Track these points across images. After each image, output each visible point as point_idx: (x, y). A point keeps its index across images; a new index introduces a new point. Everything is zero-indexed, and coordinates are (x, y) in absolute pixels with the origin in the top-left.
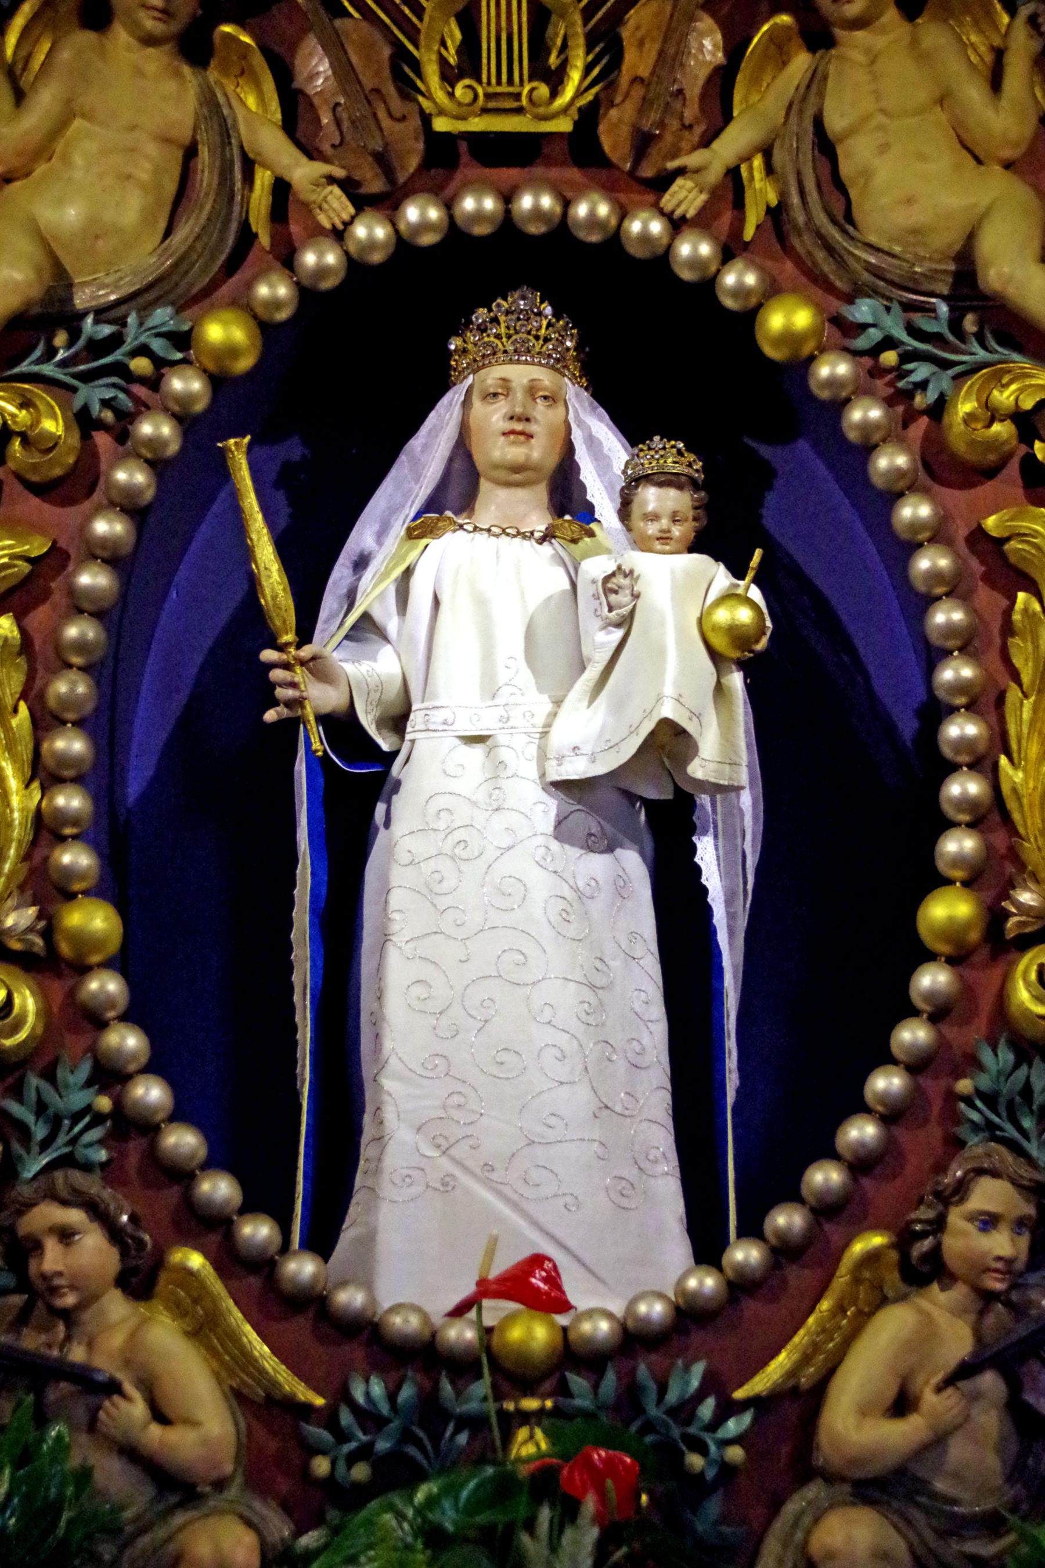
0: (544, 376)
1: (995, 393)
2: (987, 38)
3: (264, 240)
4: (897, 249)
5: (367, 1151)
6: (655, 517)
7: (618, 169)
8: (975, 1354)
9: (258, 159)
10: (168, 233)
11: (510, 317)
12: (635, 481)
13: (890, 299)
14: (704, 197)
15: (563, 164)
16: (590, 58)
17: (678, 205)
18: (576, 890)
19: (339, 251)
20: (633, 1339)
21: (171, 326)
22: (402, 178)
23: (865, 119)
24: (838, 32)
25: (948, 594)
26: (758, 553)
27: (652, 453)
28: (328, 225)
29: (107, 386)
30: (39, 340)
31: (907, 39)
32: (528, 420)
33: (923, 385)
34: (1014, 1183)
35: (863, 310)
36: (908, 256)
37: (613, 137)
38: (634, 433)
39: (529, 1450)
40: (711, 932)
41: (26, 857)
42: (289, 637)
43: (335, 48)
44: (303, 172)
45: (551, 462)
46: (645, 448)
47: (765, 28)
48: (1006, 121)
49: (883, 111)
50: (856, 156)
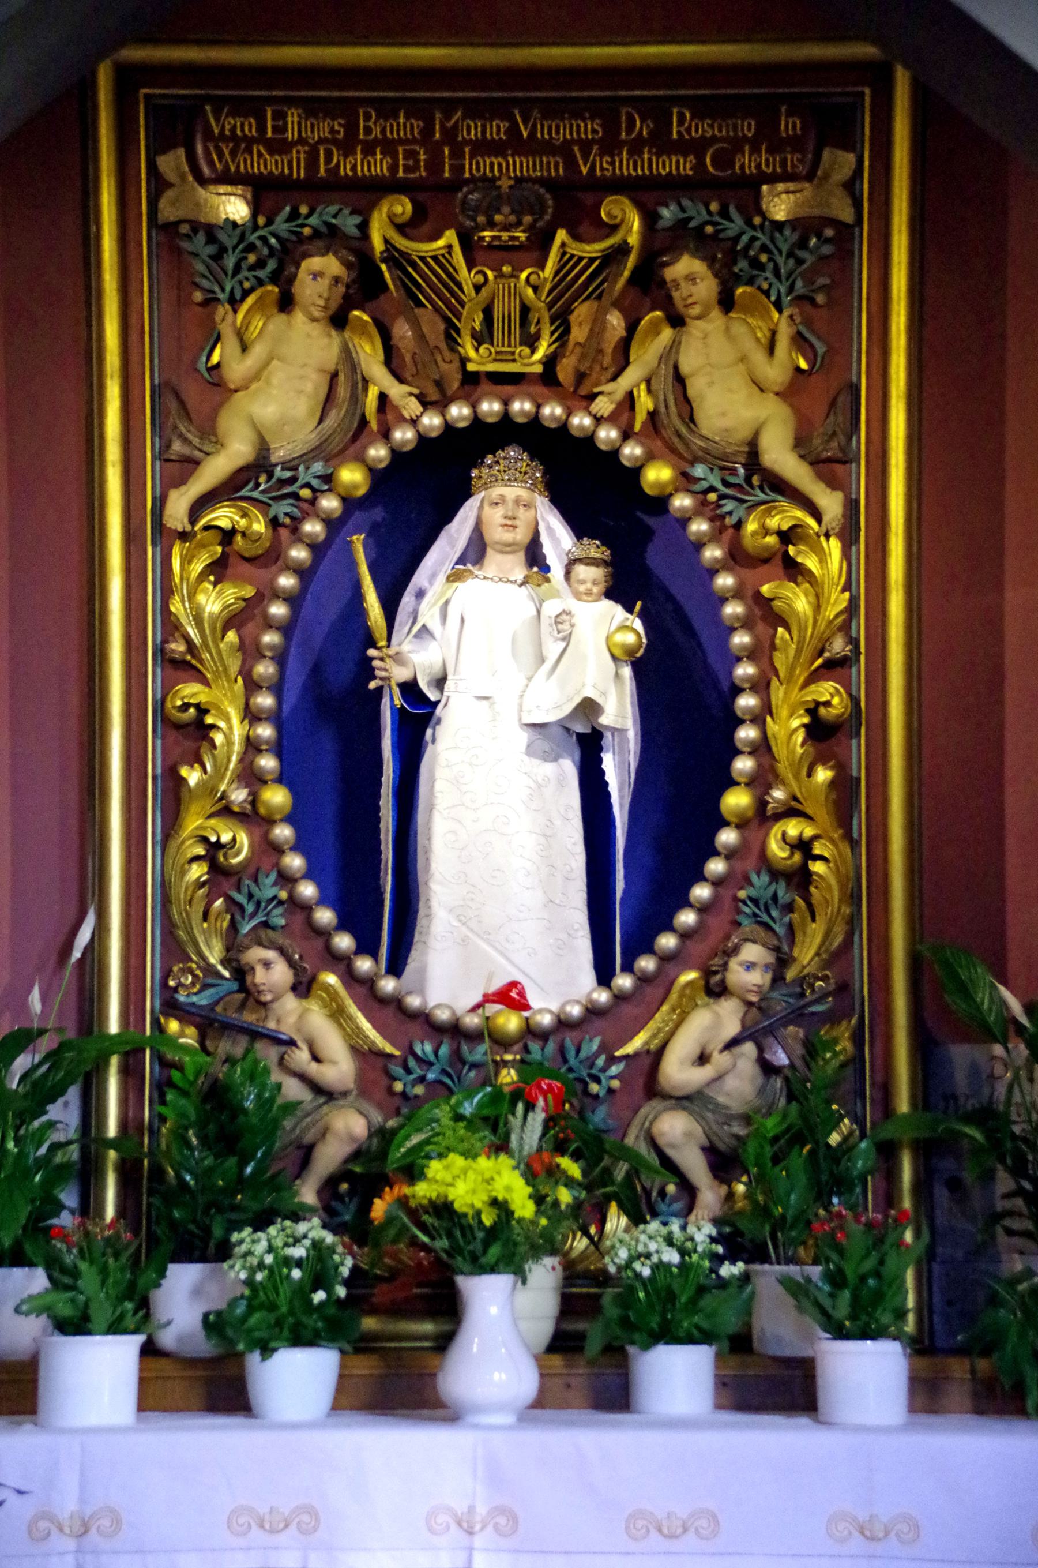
1: (768, 521)
3: (374, 425)
4: (717, 439)
5: (421, 921)
6: (583, 582)
8: (741, 1032)
10: (321, 421)
16: (553, 328)
18: (536, 782)
20: (563, 1023)
22: (449, 393)
24: (688, 320)
25: (742, 627)
31: (723, 327)
33: (730, 513)
34: (763, 945)
35: (699, 471)
36: (723, 443)
37: (565, 371)
39: (508, 1080)
40: (609, 806)
41: (241, 761)
42: (383, 643)
43: (415, 324)
44: (396, 391)
45: (527, 540)
48: (775, 372)
49: (710, 364)
50: (695, 387)
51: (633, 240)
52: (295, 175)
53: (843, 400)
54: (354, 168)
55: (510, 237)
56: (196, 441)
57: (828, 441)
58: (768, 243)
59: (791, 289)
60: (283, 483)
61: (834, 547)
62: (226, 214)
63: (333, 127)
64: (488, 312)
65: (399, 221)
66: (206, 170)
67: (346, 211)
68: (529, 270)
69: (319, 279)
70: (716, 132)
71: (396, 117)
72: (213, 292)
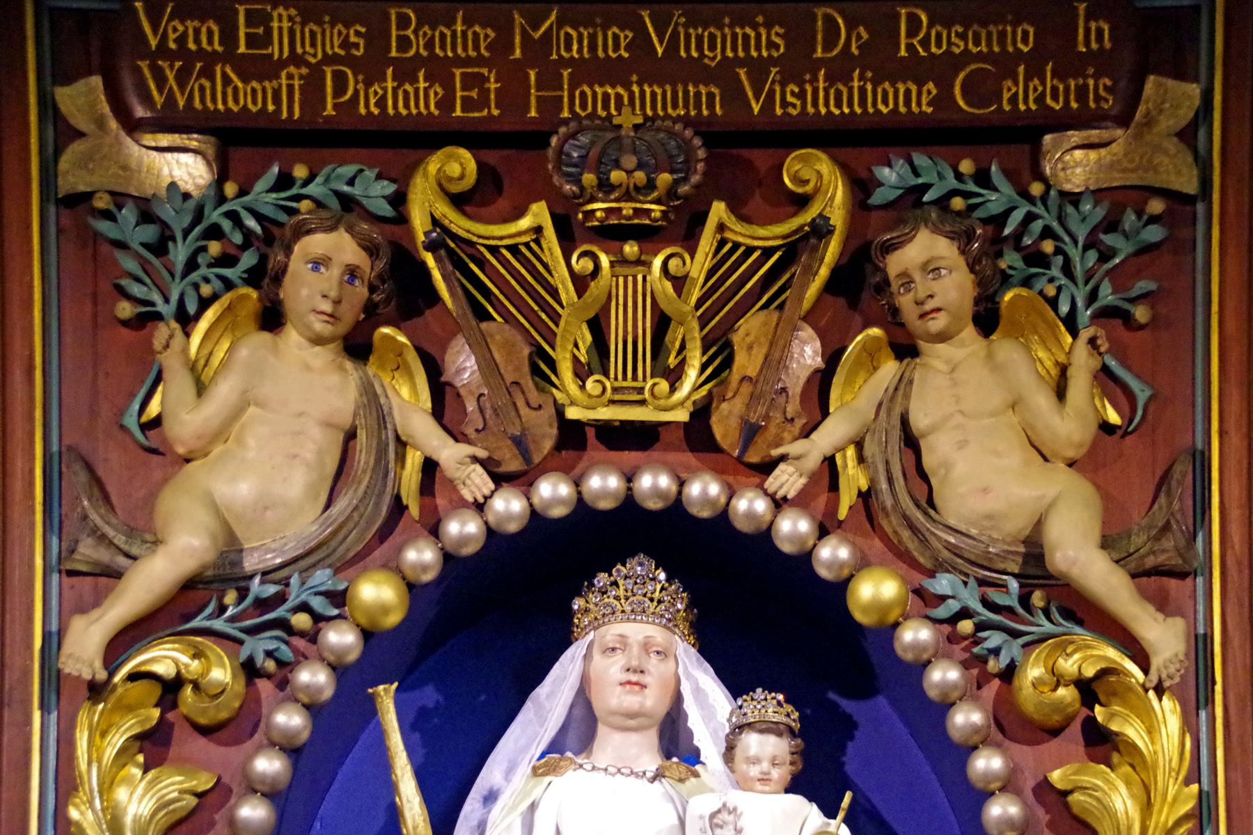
0: (654, 632)
1: (1061, 661)
2: (1053, 354)
3: (414, 511)
4: (974, 532)
6: (756, 761)
7: (728, 454)
9: (410, 441)
10: (328, 506)
11: (628, 581)
12: (739, 728)
13: (967, 575)
14: (803, 481)
15: (678, 449)
17: (781, 487)
19: (479, 520)
21: (329, 586)
22: (537, 459)
23: (947, 418)
24: (922, 345)
26: (848, 797)
27: (755, 703)
28: (471, 499)
29: (271, 638)
30: (211, 600)
31: (983, 353)
32: (642, 672)
33: (996, 652)
35: (943, 584)
36: (983, 538)
37: (724, 426)
38: (737, 687)
43: (481, 347)
44: (450, 453)
46: (749, 699)
47: (859, 338)
48: (1070, 426)
49: (961, 412)
51: (838, 218)
52: (285, 115)
53: (1183, 469)
54: (381, 103)
55: (635, 209)
56: (120, 540)
57: (1157, 538)
58: (1055, 225)
59: (1092, 297)
60: (263, 605)
61: (1168, 711)
62: (172, 176)
63: (348, 36)
64: (598, 326)
65: (455, 188)
66: (140, 112)
67: (370, 174)
68: (668, 251)
69: (323, 269)
70: (970, 45)
71: (450, 23)
72: (153, 304)
